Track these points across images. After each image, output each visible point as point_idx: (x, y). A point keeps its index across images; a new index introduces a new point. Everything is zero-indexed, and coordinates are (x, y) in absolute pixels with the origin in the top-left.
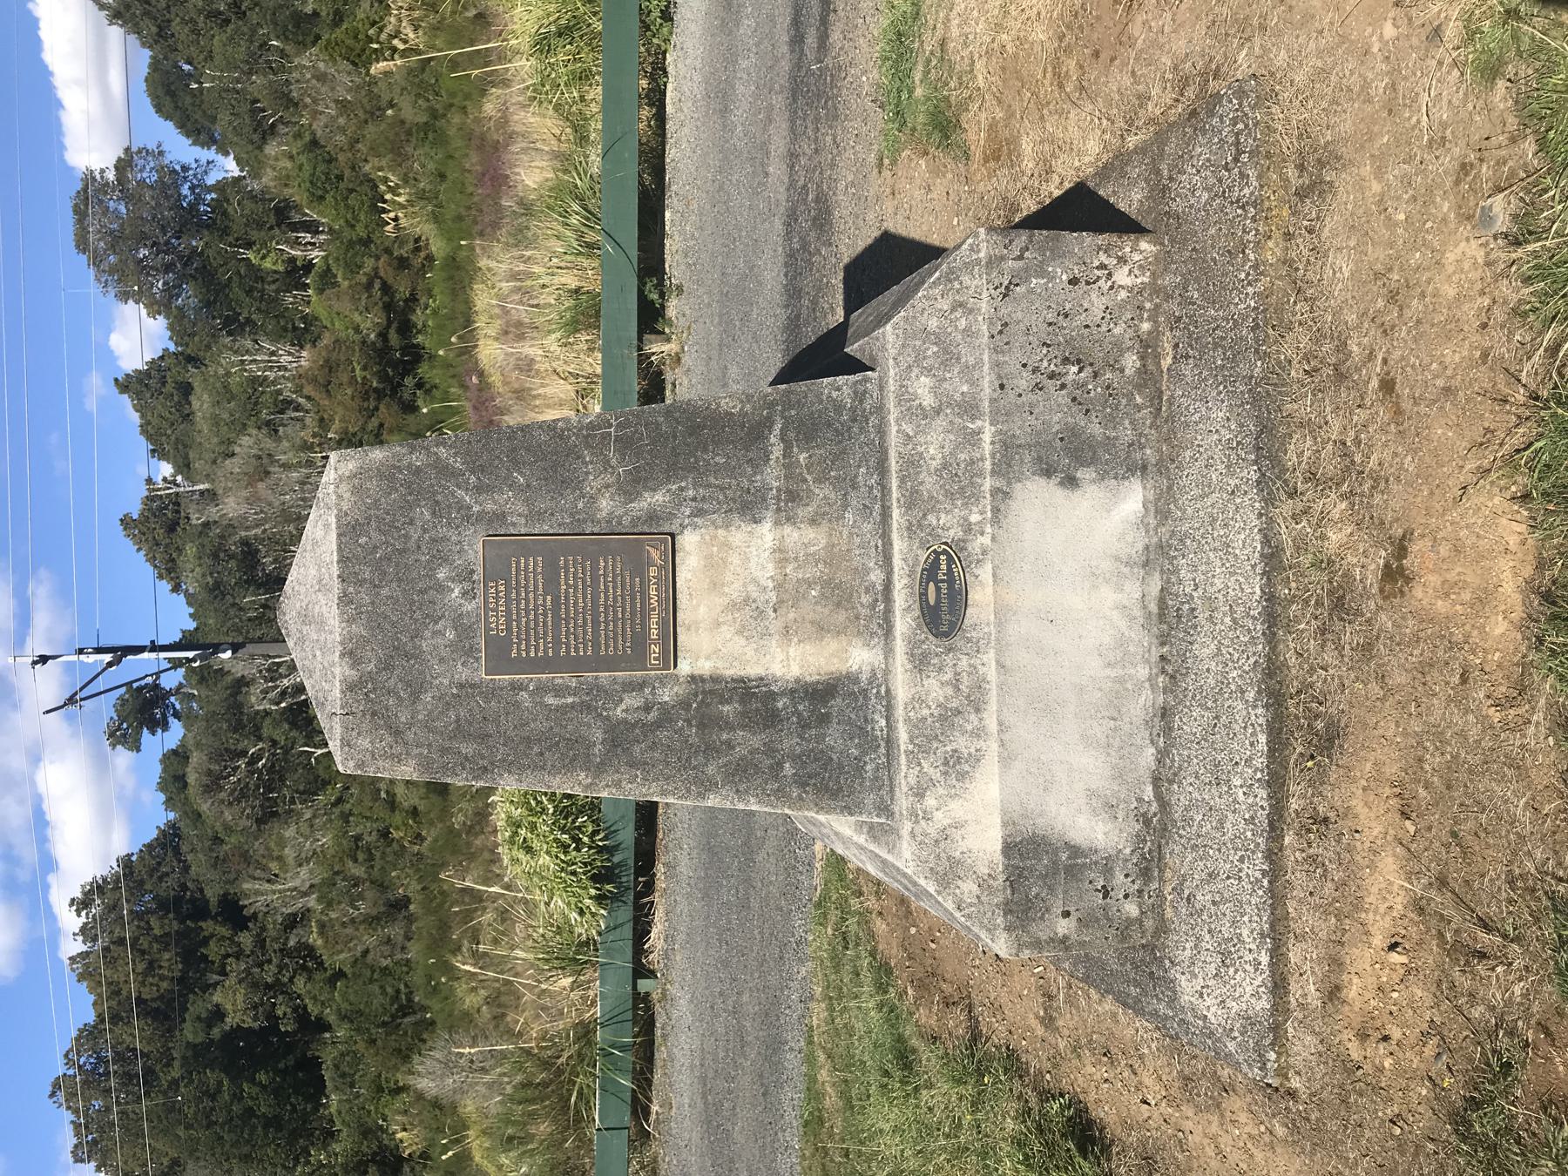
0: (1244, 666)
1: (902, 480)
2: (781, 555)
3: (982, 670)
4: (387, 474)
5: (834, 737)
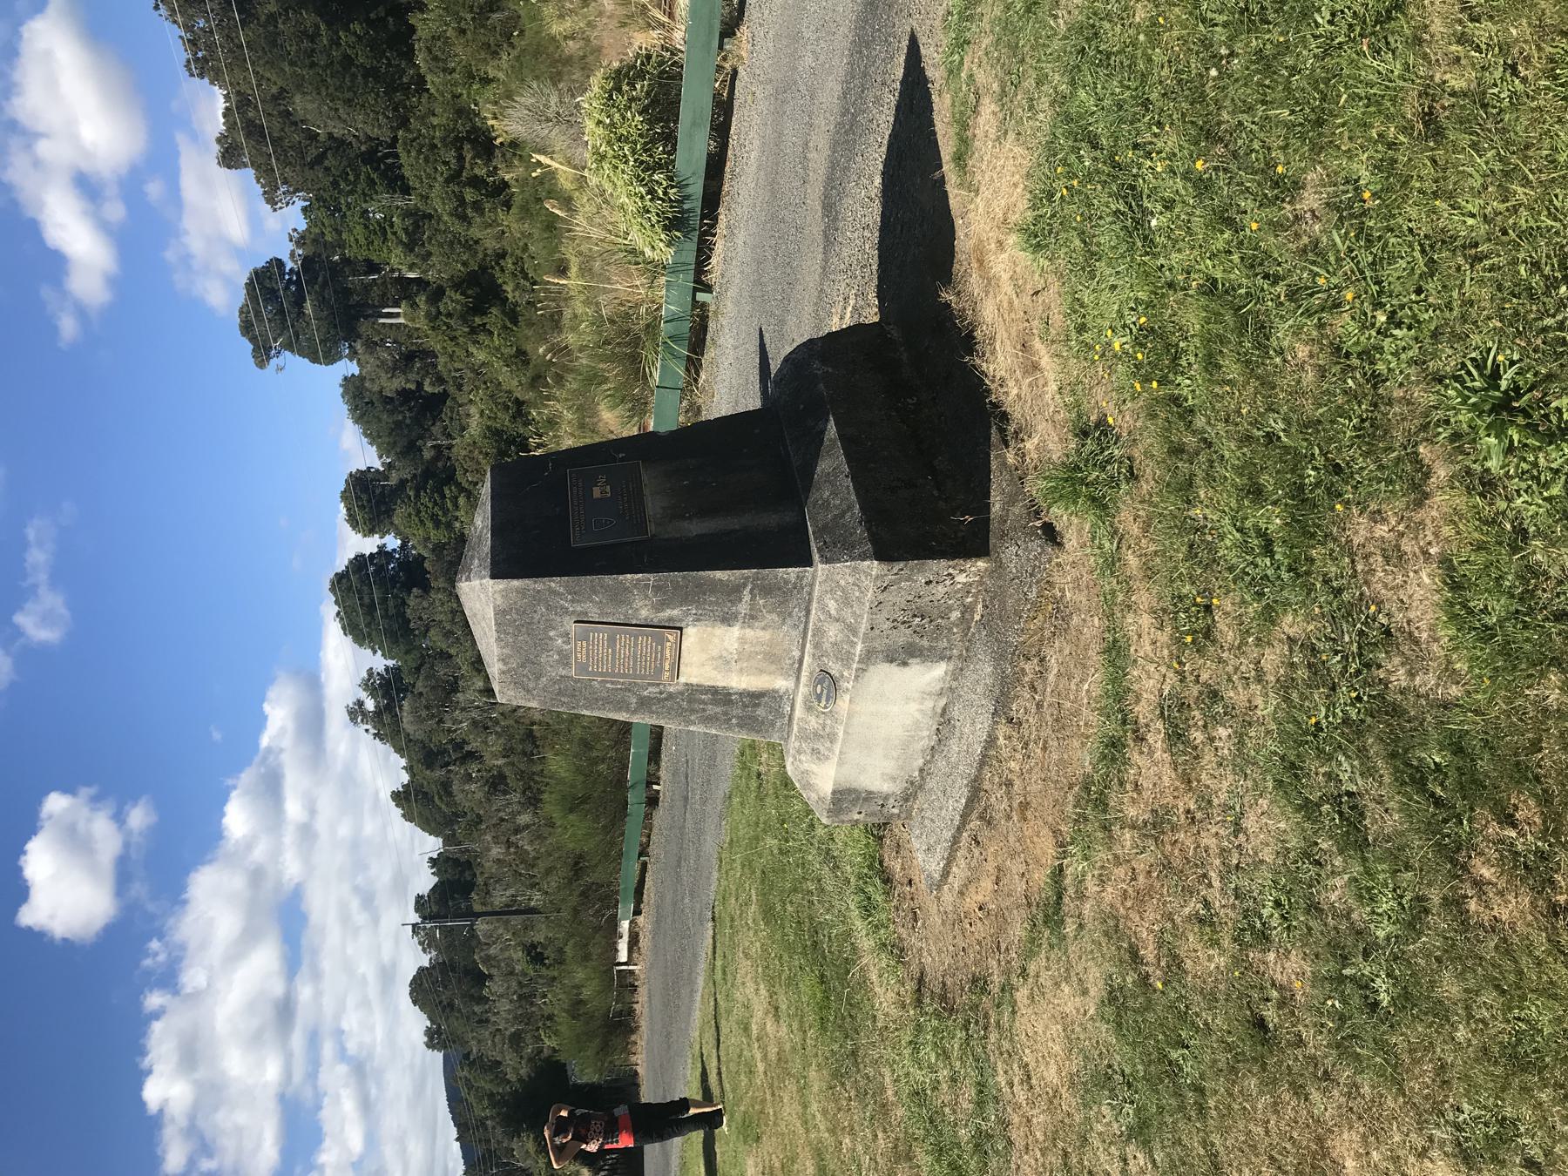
0: (967, 769)
2: (743, 641)
4: (522, 592)
5: (761, 712)
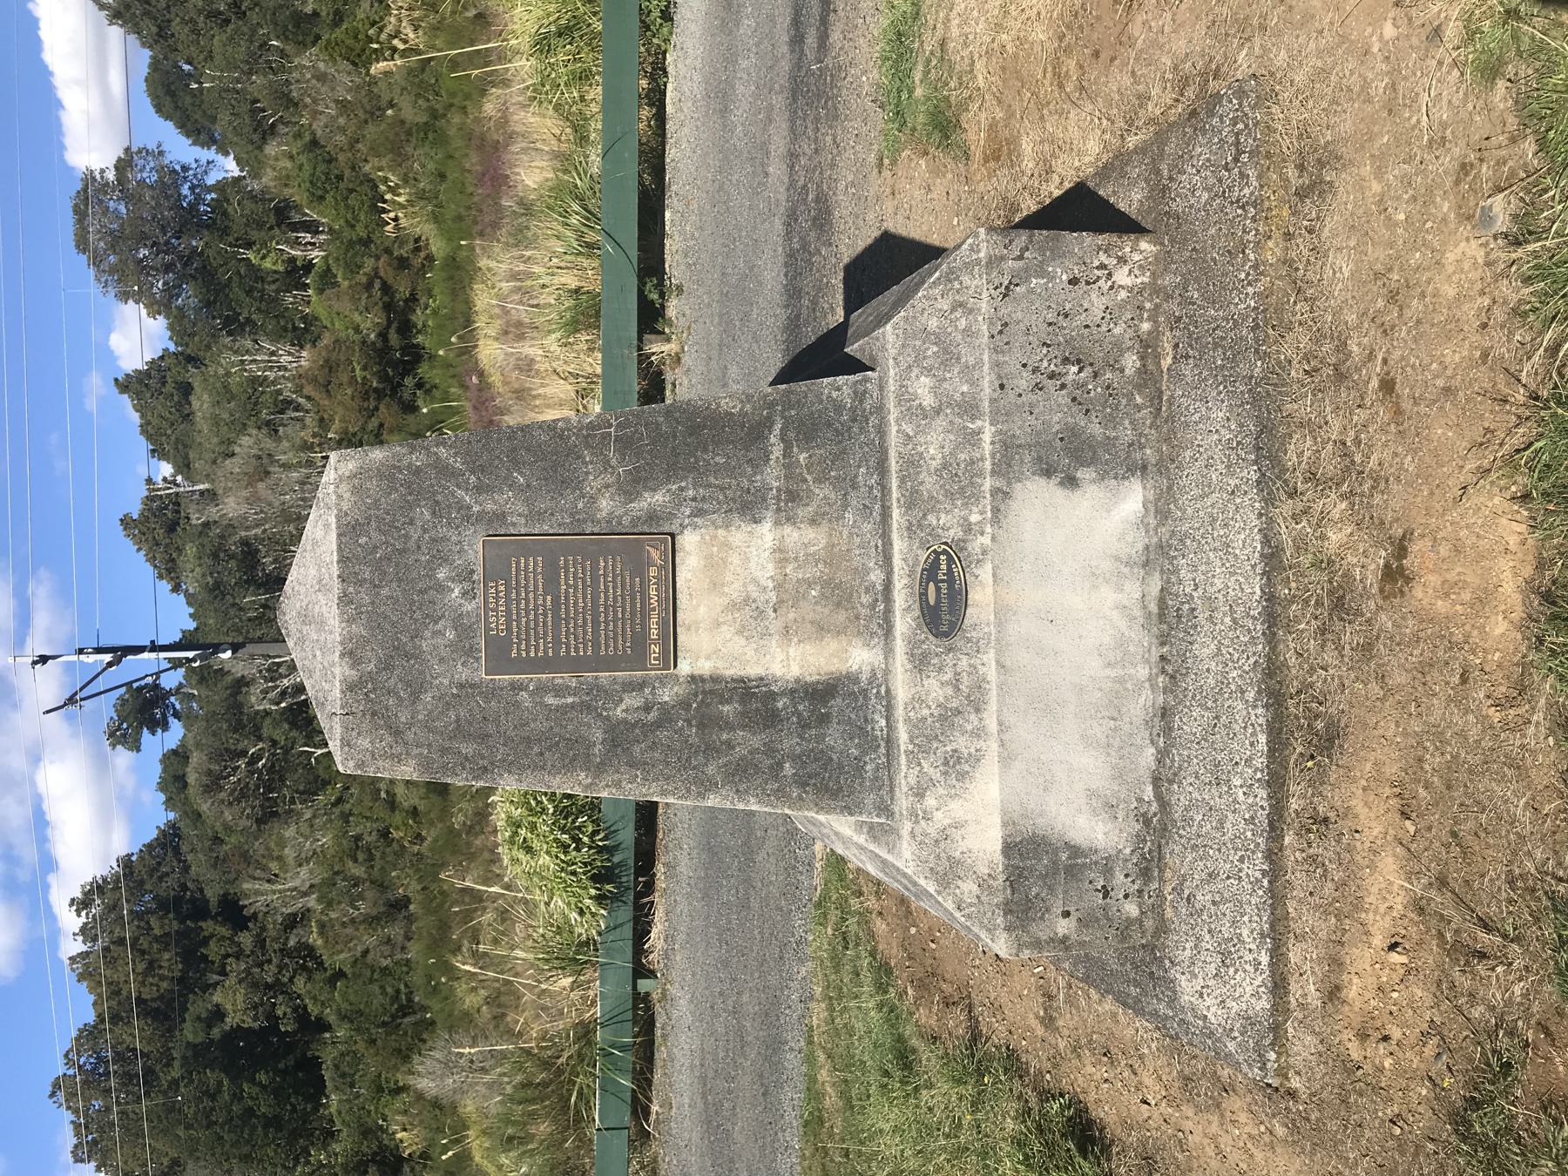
0: (1244, 666)
1: (902, 480)
2: (781, 555)
3: (982, 670)
4: (387, 474)
5: (834, 737)
